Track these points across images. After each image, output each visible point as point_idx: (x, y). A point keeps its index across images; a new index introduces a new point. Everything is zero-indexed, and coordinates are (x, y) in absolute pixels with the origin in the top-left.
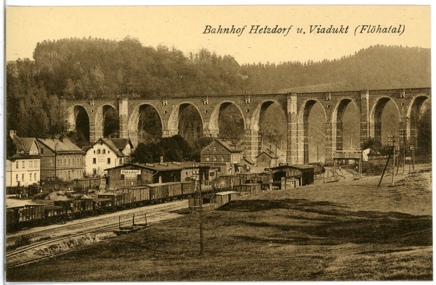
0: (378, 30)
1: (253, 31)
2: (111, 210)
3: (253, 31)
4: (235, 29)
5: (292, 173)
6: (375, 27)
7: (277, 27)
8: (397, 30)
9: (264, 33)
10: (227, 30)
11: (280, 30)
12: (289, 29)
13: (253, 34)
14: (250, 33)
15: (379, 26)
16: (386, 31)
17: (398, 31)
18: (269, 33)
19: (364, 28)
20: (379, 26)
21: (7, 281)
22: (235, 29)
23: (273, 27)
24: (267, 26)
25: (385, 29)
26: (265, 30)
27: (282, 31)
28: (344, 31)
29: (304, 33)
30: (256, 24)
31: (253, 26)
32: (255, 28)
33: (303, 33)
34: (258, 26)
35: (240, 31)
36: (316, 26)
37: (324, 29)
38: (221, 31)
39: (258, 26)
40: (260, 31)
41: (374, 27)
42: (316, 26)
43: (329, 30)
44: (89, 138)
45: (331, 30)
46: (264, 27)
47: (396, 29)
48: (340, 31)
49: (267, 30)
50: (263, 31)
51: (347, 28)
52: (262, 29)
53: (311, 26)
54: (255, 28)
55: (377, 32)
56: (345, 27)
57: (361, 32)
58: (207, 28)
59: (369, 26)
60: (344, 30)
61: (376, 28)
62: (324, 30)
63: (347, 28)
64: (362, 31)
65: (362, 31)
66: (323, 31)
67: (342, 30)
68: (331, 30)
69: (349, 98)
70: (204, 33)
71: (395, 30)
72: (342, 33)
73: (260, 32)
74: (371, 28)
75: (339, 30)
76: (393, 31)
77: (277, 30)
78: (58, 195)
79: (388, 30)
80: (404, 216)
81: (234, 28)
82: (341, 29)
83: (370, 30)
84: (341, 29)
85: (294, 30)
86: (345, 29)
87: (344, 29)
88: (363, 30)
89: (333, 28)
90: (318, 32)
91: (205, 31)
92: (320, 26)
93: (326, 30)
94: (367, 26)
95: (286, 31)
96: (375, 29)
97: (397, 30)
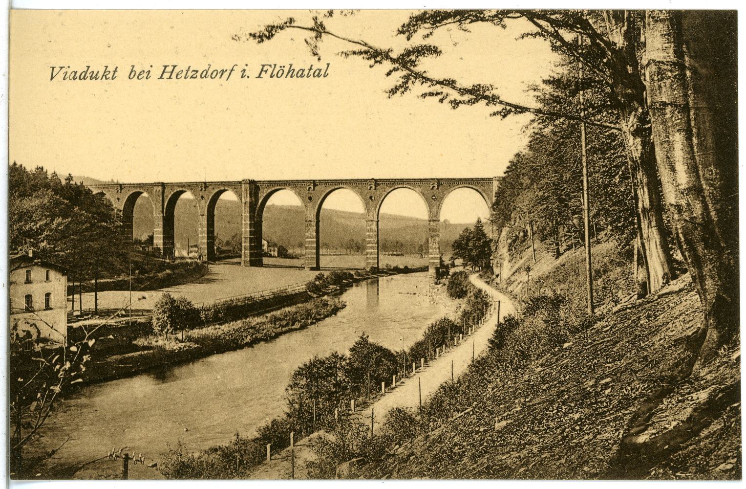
1: (166, 75)
4: (294, 70)
5: (22, 327)
6: (284, 67)
8: (322, 72)
9: (185, 78)
10: (93, 76)
12: (232, 70)
14: (161, 77)
16: (302, 74)
17: (113, 77)
19: (265, 69)
21: (13, 477)
24: (190, 67)
25: (73, 74)
27: (219, 75)
28: (110, 76)
30: (171, 63)
31: (166, 67)
32: (169, 69)
35: (109, 74)
36: (61, 68)
37: (76, 73)
38: (293, 73)
39: (175, 67)
40: (177, 75)
41: (282, 68)
42: (61, 68)
43: (205, 72)
45: (87, 75)
46: (185, 68)
47: (320, 70)
48: (103, 75)
50: (183, 74)
51: (115, 71)
53: (53, 68)
54: (169, 69)
55: (286, 77)
56: (111, 69)
57: (259, 77)
59: (273, 66)
60: (109, 74)
61: (286, 70)
63: (115, 71)
64: (261, 73)
65: (261, 73)
67: (106, 74)
68: (87, 75)
69: (141, 191)
72: (106, 79)
73: (140, 77)
74: (278, 68)
75: (100, 75)
76: (82, 77)
77: (209, 73)
78: (645, 80)
79: (306, 73)
81: (292, 69)
83: (275, 73)
84: (105, 72)
85: (237, 73)
86: (112, 73)
87: (110, 72)
90: (64, 79)
93: (78, 75)
94: (270, 66)
95: (226, 74)
96: (283, 71)
97: (322, 72)
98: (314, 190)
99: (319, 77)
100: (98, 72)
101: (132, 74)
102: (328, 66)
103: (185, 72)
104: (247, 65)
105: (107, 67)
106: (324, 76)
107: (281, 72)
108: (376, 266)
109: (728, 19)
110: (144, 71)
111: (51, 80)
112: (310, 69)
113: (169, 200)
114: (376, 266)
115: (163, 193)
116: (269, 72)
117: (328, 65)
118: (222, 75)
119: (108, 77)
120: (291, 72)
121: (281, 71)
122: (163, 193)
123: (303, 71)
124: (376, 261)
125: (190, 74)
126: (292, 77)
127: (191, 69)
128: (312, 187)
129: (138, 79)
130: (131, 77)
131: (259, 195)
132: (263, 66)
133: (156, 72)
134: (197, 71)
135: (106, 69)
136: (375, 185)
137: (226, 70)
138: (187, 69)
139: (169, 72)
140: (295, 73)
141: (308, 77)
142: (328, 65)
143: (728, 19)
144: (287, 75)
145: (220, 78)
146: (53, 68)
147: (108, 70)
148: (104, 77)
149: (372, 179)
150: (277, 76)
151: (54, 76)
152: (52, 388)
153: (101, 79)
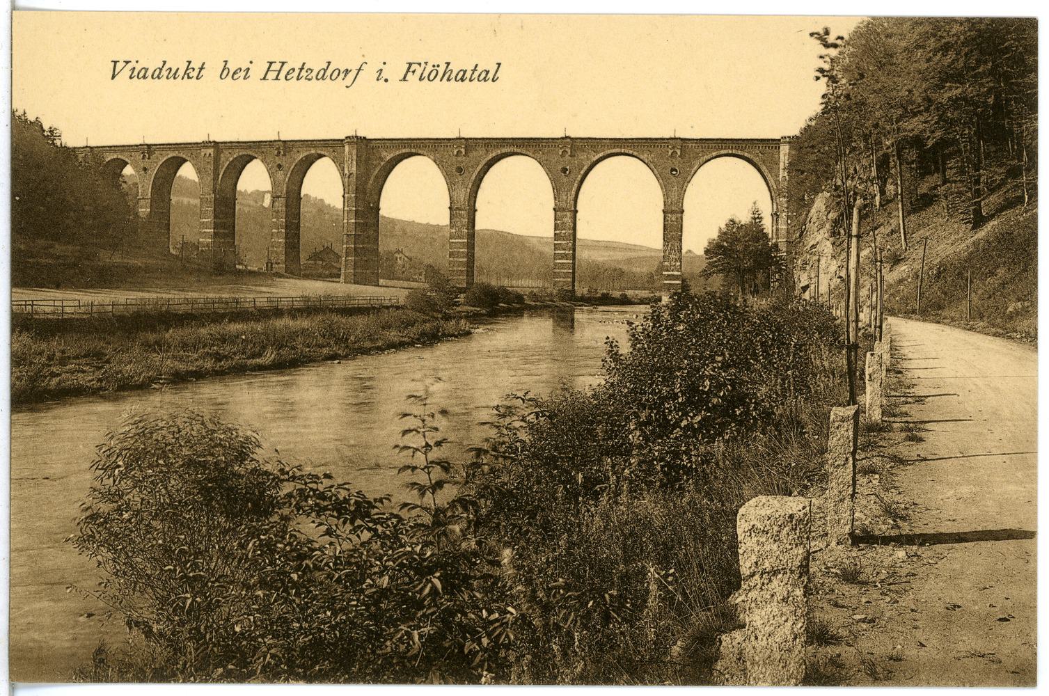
0: (444, 75)
1: (272, 75)
2: (376, 637)
3: (272, 75)
4: (452, 71)
6: (438, 66)
8: (491, 75)
9: (298, 79)
11: (431, 78)
12: (359, 70)
13: (270, 82)
15: (448, 64)
18: (309, 80)
19: (412, 69)
20: (448, 64)
23: (317, 65)
24: (304, 64)
26: (299, 74)
27: (342, 75)
28: (194, 74)
29: (386, 80)
31: (271, 63)
32: (276, 67)
33: (383, 80)
34: (283, 63)
35: (192, 72)
36: (127, 62)
39: (283, 63)
40: (288, 73)
41: (436, 68)
42: (127, 62)
45: (164, 72)
46: (298, 66)
47: (487, 72)
50: (295, 74)
53: (115, 62)
54: (276, 67)
55: (441, 80)
57: (404, 79)
58: (270, 66)
60: (192, 72)
62: (160, 72)
63: (201, 69)
67: (188, 72)
68: (164, 72)
72: (189, 77)
73: (235, 77)
74: (429, 68)
75: (181, 73)
76: (155, 76)
77: (328, 73)
79: (468, 75)
80: (969, 641)
82: (187, 69)
83: (426, 74)
85: (369, 73)
86: (197, 71)
88: (410, 74)
89: (167, 66)
90: (131, 78)
94: (420, 64)
95: (351, 76)
97: (491, 75)
100: (178, 69)
101: (226, 72)
102: (499, 67)
103: (297, 71)
106: (493, 81)
108: (570, 288)
109: (1029, 26)
110: (241, 69)
111: (113, 79)
114: (570, 288)
116: (418, 73)
118: (345, 76)
120: (447, 75)
121: (434, 72)
123: (465, 72)
124: (570, 280)
130: (223, 77)
132: (410, 64)
133: (258, 70)
134: (312, 70)
135: (447, 67)
140: (453, 76)
141: (471, 80)
142: (499, 64)
143: (1029, 26)
144: (443, 77)
146: (115, 62)
147: (450, 68)
148: (186, 76)
149: (206, 144)
150: (429, 79)
151: (117, 70)
152: (466, 651)
153: (183, 79)
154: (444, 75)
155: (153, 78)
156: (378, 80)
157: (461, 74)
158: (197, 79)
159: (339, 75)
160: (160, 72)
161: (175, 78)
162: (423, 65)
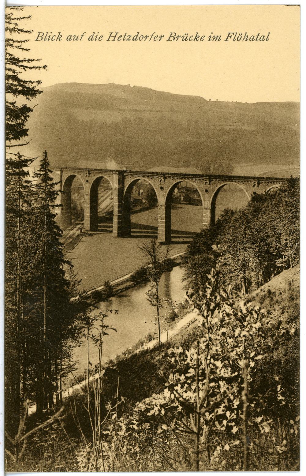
0: (244, 38)
1: (112, 39)
3: (112, 39)
4: (248, 36)
6: (242, 34)
7: (94, 35)
8: (265, 38)
9: (124, 40)
14: (108, 40)
15: (246, 33)
17: (257, 39)
19: (230, 36)
20: (246, 33)
22: (248, 36)
24: (126, 33)
27: (144, 39)
31: (111, 33)
32: (114, 35)
39: (117, 33)
41: (241, 35)
44: (295, 331)
46: (123, 35)
47: (264, 37)
48: (58, 38)
49: (127, 38)
50: (122, 38)
52: (121, 36)
54: (114, 35)
57: (226, 40)
59: (235, 34)
62: (71, 37)
64: (227, 39)
65: (227, 39)
66: (92, 39)
67: (197, 37)
70: (37, 40)
71: (92, 38)
72: (197, 41)
73: (155, 39)
74: (238, 35)
76: (90, 39)
77: (138, 37)
79: (255, 38)
81: (246, 35)
83: (236, 38)
84: (59, 36)
88: (229, 38)
91: (37, 38)
92: (51, 33)
94: (233, 33)
95: (148, 38)
97: (265, 38)
98: (164, 182)
99: (70, 40)
101: (218, 38)
103: (123, 37)
104: (212, 33)
105: (60, 33)
106: (267, 40)
107: (240, 37)
112: (258, 36)
113: (170, 190)
115: (61, 176)
117: (269, 33)
119: (198, 39)
120: (246, 38)
122: (61, 176)
123: (254, 37)
125: (126, 37)
126: (246, 40)
127: (127, 35)
128: (163, 180)
129: (118, 40)
131: (99, 189)
132: (229, 33)
133: (224, 37)
135: (197, 35)
136: (164, 179)
137: (180, 36)
138: (124, 35)
139: (173, 37)
140: (249, 38)
142: (269, 33)
145: (177, 40)
148: (58, 39)
150: (237, 40)
153: (194, 41)
154: (244, 38)
155: (260, 40)
156: (209, 41)
157: (252, 38)
158: (253, 40)
159: (143, 38)
160: (71, 37)
161: (186, 40)
162: (235, 34)
